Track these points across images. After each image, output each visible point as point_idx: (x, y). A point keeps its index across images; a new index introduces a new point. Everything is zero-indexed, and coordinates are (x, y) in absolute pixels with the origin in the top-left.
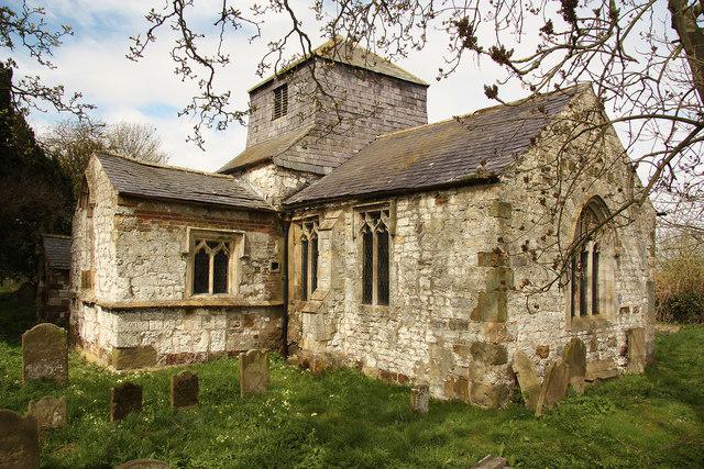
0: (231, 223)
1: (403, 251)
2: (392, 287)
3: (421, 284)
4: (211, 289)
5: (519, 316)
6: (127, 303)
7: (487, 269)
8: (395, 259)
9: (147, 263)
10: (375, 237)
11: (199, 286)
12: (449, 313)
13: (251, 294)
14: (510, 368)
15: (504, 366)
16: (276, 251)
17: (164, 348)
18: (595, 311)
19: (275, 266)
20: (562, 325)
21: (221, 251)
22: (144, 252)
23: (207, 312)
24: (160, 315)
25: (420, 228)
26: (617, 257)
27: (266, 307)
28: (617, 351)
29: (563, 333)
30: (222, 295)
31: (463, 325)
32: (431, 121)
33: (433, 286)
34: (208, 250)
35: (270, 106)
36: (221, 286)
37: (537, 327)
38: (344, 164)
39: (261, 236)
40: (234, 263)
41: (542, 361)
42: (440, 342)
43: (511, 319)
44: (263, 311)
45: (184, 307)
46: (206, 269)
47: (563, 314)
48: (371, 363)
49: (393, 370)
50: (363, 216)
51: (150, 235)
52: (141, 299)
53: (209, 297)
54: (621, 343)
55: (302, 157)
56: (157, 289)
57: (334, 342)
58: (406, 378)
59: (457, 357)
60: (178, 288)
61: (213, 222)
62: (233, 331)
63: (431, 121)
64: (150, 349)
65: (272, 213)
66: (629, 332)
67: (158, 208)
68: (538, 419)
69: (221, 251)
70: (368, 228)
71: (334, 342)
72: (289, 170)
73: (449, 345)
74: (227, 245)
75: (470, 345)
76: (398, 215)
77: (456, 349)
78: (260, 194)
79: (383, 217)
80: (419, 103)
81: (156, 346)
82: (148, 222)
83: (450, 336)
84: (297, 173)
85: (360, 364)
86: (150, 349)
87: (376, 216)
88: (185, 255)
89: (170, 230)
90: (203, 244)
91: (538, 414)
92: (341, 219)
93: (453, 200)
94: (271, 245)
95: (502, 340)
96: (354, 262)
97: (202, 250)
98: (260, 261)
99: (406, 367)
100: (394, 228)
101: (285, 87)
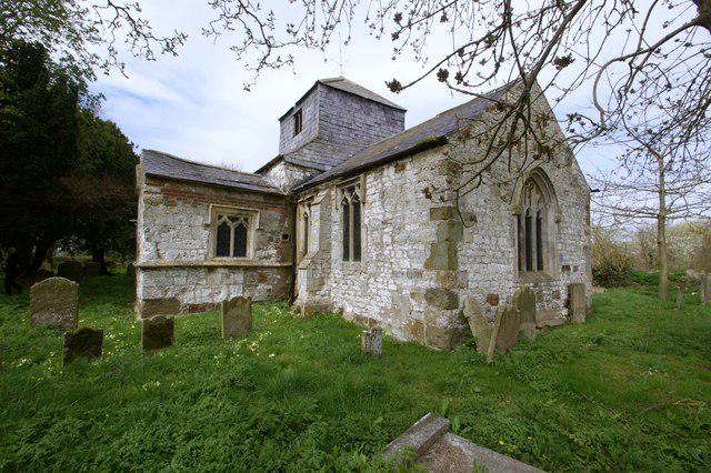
0: (249, 203)
1: (371, 214)
2: (363, 245)
3: (385, 240)
4: (232, 253)
5: (469, 266)
6: (153, 263)
7: (437, 222)
8: (365, 221)
9: (172, 232)
10: (351, 207)
11: (222, 249)
12: (406, 264)
13: (266, 257)
14: (462, 313)
15: (456, 311)
16: (286, 225)
17: (187, 299)
18: (540, 267)
19: (285, 237)
20: (511, 277)
21: (241, 225)
22: (170, 222)
23: (226, 271)
24: (185, 273)
25: (383, 194)
26: (558, 222)
27: (277, 267)
28: (561, 303)
29: (511, 284)
30: (240, 259)
31: (419, 274)
32: (407, 128)
33: (393, 242)
34: (229, 223)
35: (292, 127)
36: (241, 250)
37: (491, 270)
38: (335, 162)
39: (275, 214)
40: (252, 236)
41: (493, 308)
42: (399, 290)
43: (461, 268)
44: (275, 270)
45: (205, 267)
46: (229, 239)
47: (512, 266)
48: (349, 309)
49: (365, 315)
50: (343, 191)
51: (175, 209)
52: (167, 260)
53: (230, 260)
54: (564, 296)
55: (308, 156)
56: (182, 252)
57: (322, 292)
58: (375, 322)
59: (413, 302)
60: (201, 251)
61: (232, 201)
62: (249, 286)
63: (407, 128)
64: (174, 301)
65: (282, 197)
66: (570, 288)
67: (183, 188)
68: (490, 365)
69: (241, 225)
70: (346, 200)
71: (322, 292)
72: (297, 166)
73: (406, 292)
74: (246, 220)
75: (424, 292)
76: (367, 186)
77: (413, 295)
78: (276, 185)
79: (357, 190)
80: (399, 123)
81: (180, 297)
82: (175, 199)
83: (408, 284)
84: (304, 168)
85: (342, 311)
86: (174, 301)
87: (351, 190)
88: (207, 226)
89: (194, 206)
90: (225, 218)
91: (489, 360)
92: (328, 196)
93: (408, 167)
94: (282, 221)
95: (453, 287)
96: (337, 230)
97: (225, 223)
98: (273, 233)
99: (373, 312)
100: (364, 198)
101: (300, 112)
